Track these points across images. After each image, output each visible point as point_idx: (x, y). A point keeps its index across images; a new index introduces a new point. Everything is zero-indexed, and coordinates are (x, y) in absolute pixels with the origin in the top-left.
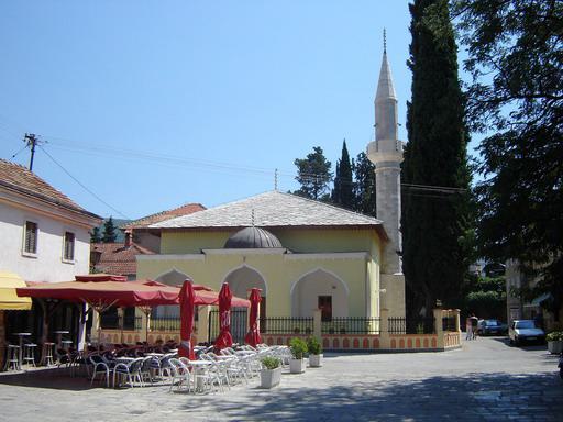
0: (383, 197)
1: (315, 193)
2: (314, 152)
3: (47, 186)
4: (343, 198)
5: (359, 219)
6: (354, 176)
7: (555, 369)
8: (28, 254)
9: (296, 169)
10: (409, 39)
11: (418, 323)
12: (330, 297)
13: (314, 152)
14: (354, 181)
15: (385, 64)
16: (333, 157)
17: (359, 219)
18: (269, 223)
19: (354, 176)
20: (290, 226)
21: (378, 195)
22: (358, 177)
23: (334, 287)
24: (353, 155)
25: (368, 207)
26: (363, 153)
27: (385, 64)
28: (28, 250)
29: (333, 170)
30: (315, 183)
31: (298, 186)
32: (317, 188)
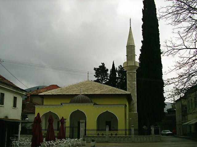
0: (129, 83)
1: (102, 81)
2: (102, 65)
3: (5, 79)
4: (112, 82)
5: (122, 92)
6: (117, 74)
7: (165, 102)
8: (14, 108)
9: (95, 71)
10: (142, 29)
11: (129, 120)
12: (111, 121)
13: (102, 65)
14: (117, 76)
15: (130, 32)
16: (109, 67)
17: (122, 92)
18: (86, 93)
19: (117, 74)
20: (95, 94)
21: (128, 82)
22: (118, 75)
23: (112, 118)
24: (117, 66)
25: (123, 86)
26: (121, 66)
27: (130, 32)
28: (14, 107)
29: (109, 72)
30: (102, 78)
31: (96, 79)
32: (103, 79)
